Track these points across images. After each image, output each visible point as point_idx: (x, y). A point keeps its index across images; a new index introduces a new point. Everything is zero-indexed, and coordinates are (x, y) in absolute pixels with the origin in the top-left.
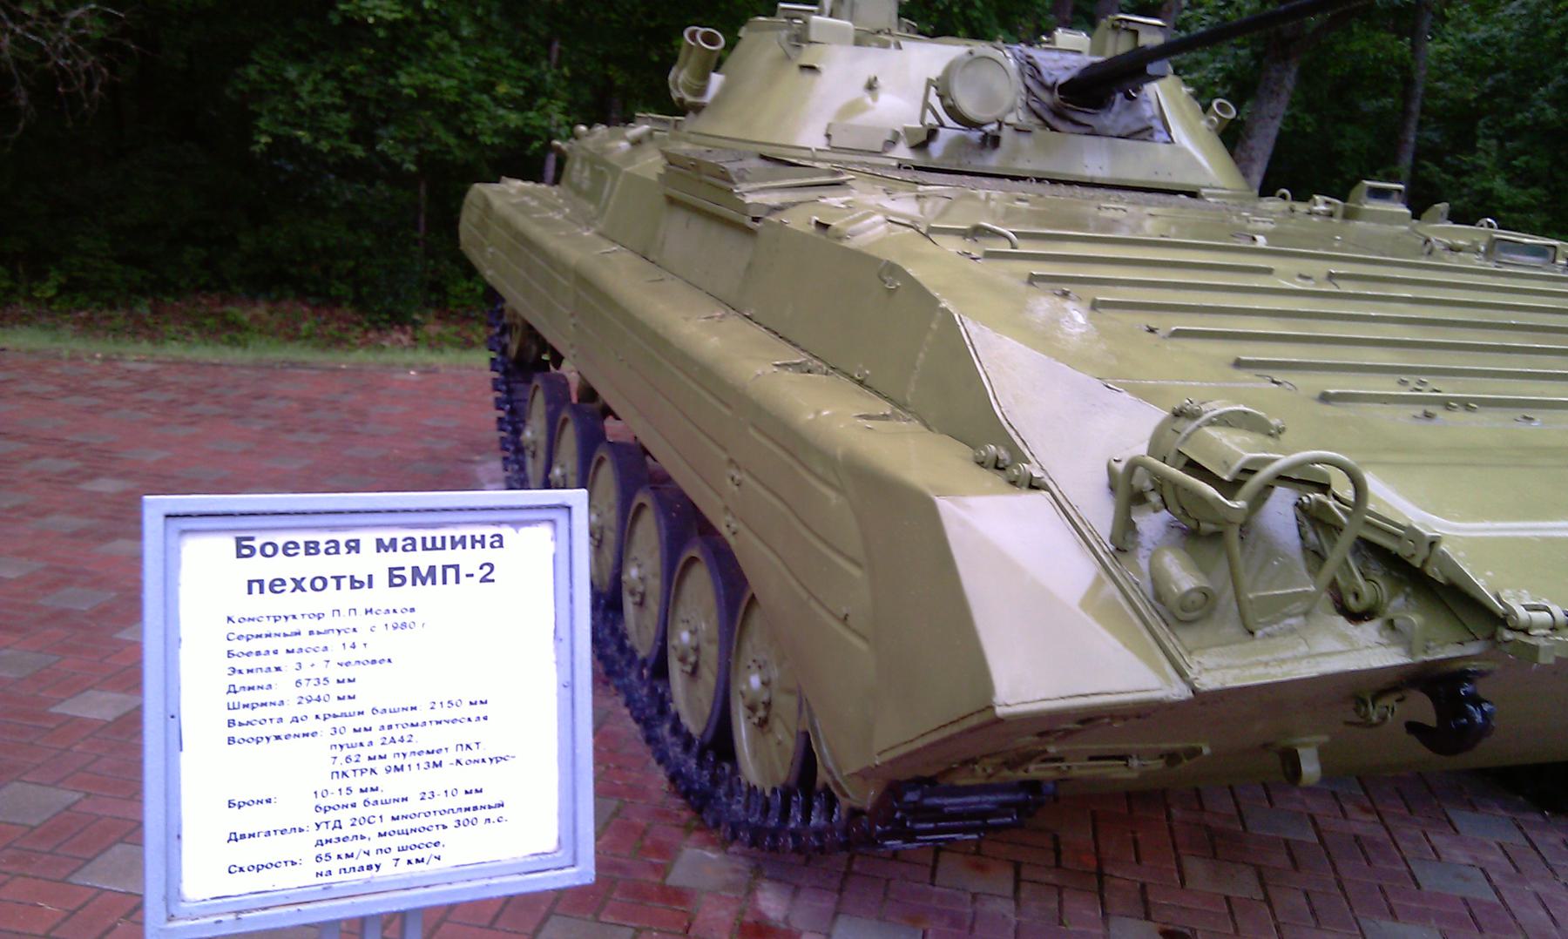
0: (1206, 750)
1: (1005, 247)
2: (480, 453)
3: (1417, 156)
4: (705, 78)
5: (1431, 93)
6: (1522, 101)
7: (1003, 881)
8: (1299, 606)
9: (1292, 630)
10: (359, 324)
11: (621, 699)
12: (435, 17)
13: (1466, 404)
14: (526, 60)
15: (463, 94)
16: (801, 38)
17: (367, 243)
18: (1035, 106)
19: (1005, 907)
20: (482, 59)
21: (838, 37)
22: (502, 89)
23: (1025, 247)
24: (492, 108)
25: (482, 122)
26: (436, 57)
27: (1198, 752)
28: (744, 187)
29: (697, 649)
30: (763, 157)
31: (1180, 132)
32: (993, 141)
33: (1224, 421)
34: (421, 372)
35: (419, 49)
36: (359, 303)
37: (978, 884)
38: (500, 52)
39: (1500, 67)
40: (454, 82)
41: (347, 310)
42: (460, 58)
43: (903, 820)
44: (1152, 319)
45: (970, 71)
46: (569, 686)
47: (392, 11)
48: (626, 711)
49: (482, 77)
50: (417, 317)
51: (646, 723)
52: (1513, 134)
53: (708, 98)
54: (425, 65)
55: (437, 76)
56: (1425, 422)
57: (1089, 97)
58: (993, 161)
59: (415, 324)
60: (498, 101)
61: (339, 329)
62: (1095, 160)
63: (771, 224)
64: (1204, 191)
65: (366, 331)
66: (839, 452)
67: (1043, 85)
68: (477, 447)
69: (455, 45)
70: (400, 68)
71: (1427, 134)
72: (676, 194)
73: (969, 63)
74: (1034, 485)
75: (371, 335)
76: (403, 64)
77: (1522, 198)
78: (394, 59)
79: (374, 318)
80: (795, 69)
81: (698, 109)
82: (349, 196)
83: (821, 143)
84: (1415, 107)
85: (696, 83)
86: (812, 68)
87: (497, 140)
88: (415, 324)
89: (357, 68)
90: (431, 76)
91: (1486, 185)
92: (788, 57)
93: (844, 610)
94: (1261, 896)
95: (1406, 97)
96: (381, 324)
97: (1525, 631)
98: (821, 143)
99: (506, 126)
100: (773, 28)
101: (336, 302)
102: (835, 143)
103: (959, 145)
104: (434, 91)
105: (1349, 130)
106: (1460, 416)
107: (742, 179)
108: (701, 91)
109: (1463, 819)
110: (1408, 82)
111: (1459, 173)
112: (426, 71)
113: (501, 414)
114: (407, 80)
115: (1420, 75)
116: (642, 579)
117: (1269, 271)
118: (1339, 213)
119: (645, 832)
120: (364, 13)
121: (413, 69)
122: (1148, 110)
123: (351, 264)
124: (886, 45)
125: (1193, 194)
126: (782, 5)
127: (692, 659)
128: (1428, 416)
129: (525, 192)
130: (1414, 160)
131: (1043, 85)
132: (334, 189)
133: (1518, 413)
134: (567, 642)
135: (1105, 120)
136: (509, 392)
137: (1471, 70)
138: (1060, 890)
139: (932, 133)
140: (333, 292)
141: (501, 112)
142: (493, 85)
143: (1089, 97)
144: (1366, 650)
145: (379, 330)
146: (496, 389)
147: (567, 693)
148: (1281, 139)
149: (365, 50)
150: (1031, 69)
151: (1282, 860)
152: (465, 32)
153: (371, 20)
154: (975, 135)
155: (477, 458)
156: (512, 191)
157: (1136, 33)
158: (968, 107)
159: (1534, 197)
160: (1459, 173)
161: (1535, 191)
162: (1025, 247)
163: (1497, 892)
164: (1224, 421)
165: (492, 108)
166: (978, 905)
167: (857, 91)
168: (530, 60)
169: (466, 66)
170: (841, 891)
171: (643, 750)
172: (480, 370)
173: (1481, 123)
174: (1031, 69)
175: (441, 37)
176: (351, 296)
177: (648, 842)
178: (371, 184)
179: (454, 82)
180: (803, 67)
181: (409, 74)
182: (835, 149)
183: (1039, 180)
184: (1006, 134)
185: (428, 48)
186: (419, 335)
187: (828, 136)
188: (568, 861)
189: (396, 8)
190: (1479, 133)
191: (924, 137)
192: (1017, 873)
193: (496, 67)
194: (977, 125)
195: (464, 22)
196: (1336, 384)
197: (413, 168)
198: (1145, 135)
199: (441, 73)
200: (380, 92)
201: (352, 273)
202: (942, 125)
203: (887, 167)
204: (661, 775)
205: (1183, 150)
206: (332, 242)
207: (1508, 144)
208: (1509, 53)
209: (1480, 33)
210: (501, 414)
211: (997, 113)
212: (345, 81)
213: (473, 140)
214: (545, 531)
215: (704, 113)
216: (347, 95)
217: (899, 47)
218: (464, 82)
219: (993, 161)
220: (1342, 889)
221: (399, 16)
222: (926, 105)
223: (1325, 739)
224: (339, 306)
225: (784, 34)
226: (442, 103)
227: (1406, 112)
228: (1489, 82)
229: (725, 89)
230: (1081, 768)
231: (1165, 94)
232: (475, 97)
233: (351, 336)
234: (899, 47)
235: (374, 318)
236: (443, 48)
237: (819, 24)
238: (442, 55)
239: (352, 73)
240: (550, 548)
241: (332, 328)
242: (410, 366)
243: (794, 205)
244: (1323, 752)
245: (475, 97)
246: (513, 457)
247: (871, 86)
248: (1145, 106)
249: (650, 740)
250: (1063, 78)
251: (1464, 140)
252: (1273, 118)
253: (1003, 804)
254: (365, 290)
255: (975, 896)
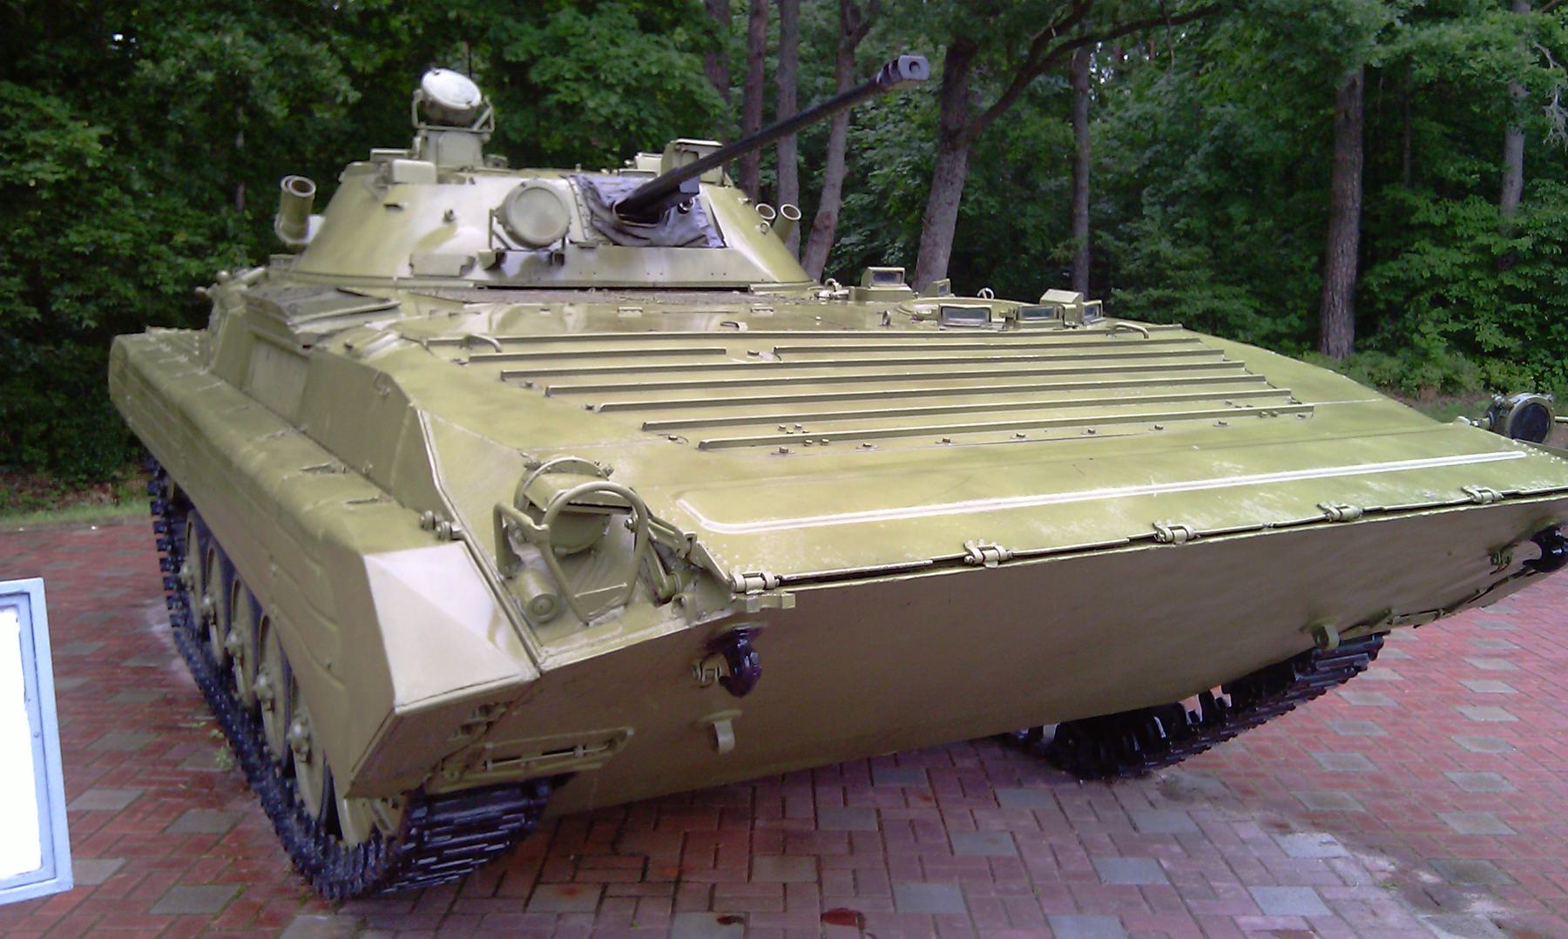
0: (630, 732)
1: (492, 352)
2: (152, 597)
3: (1093, 226)
4: (303, 221)
5: (1101, 168)
6: (1178, 168)
7: (590, 897)
8: (617, 600)
9: (615, 617)
10: (55, 487)
11: (258, 801)
12: (104, 174)
13: (819, 440)
14: (204, 208)
15: (138, 246)
16: (387, 180)
17: (58, 403)
18: (599, 225)
19: (585, 921)
20: (156, 210)
21: (421, 176)
22: (180, 238)
23: (509, 350)
24: (172, 258)
25: (161, 270)
26: (107, 213)
27: (623, 735)
28: (297, 319)
29: (308, 739)
30: (339, 291)
31: (737, 232)
32: (559, 258)
33: (558, 469)
34: (102, 527)
35: (88, 207)
36: (54, 465)
37: (565, 905)
38: (178, 201)
39: (1155, 140)
40: (128, 236)
41: (42, 475)
42: (132, 211)
43: (419, 837)
44: (590, 399)
45: (524, 200)
46: (39, 735)
47: (54, 173)
48: (262, 811)
49: (158, 228)
50: (117, 474)
51: (276, 817)
52: (1173, 199)
53: (310, 239)
54: (97, 222)
55: (109, 232)
56: (780, 457)
57: (648, 212)
58: (562, 276)
59: (114, 480)
60: (179, 252)
61: (34, 494)
62: (655, 267)
63: (318, 349)
64: (752, 287)
65: (64, 493)
66: (320, 533)
67: (602, 206)
68: (148, 592)
69: (127, 199)
70: (71, 227)
71: (1099, 207)
72: (261, 331)
73: (523, 194)
74: (454, 537)
75: (69, 498)
76: (73, 222)
77: (1185, 257)
78: (64, 219)
79: (72, 479)
80: (383, 209)
81: (297, 250)
82: (36, 360)
83: (405, 272)
84: (1084, 182)
85: (296, 227)
86: (396, 206)
87: (178, 289)
88: (114, 480)
89: (27, 231)
90: (103, 233)
91: (1154, 248)
92: (375, 199)
93: (327, 661)
94: (815, 878)
95: (1075, 174)
96: (79, 485)
97: (744, 592)
98: (405, 272)
99: (187, 274)
100: (365, 171)
101: (30, 467)
102: (417, 270)
103: (530, 264)
104: (107, 246)
105: (1030, 209)
106: (815, 449)
107: (295, 313)
108: (303, 233)
109: (1007, 795)
110: (1075, 161)
111: (1132, 240)
112: (98, 228)
113: (164, 554)
114: (78, 237)
115: (1085, 153)
116: (270, 686)
117: (723, 352)
118: (853, 296)
119: (261, 907)
120: (25, 177)
121: (83, 227)
122: (701, 222)
123: (43, 427)
124: (462, 181)
125: (744, 290)
126: (374, 151)
127: (305, 748)
128: (783, 452)
129: (168, 340)
130: (1091, 232)
131: (602, 206)
132: (18, 353)
133: (860, 443)
134: (35, 699)
135: (662, 232)
136: (171, 532)
137: (1132, 145)
138: (639, 898)
139: (500, 257)
140: (25, 458)
141: (181, 260)
142: (170, 236)
143: (648, 212)
144: (666, 623)
145: (77, 491)
146: (157, 531)
147: (39, 740)
148: (961, 219)
149: (31, 213)
150: (591, 192)
151: (843, 848)
152: (137, 187)
153: (32, 183)
154: (544, 254)
155: (149, 601)
156: (152, 339)
157: (696, 154)
158: (527, 231)
159: (1197, 254)
160: (1132, 240)
161: (1198, 249)
162: (509, 350)
163: (1018, 848)
164: (558, 469)
165: (172, 258)
166: (561, 922)
167: (435, 223)
168: (209, 207)
169: (141, 219)
170: (437, 929)
171: (273, 840)
172: (143, 517)
173: (1145, 192)
174: (591, 192)
175: (112, 192)
176: (45, 461)
177: (263, 915)
178: (58, 345)
179: (128, 236)
180: (388, 206)
181: (80, 233)
182: (418, 277)
183: (599, 289)
184: (570, 251)
185: (99, 206)
186: (120, 492)
187: (411, 265)
188: (49, 874)
189: (57, 169)
190: (1144, 201)
191: (493, 260)
192: (603, 892)
193: (173, 218)
194: (545, 246)
195: (135, 176)
196: (709, 436)
197: (93, 324)
198: (700, 242)
199: (114, 229)
200: (50, 253)
201: (44, 436)
202: (509, 249)
203: (466, 289)
204: (286, 860)
205: (735, 253)
206: (19, 407)
207: (1170, 209)
208: (1162, 127)
209: (1135, 110)
210: (164, 554)
211: (558, 232)
212: (12, 244)
213: (155, 290)
214: (10, 615)
215: (306, 254)
216: (15, 259)
217: (472, 182)
218: (140, 235)
219: (562, 276)
220: (887, 864)
221: (61, 177)
222: (492, 232)
223: (737, 712)
224: (33, 471)
225: (372, 178)
226: (117, 257)
227: (1076, 188)
228: (1148, 153)
229: (326, 228)
230: (540, 762)
231: (717, 200)
232: (152, 248)
233: (48, 501)
234: (472, 182)
235: (72, 479)
236: (114, 203)
237: (402, 167)
238: (114, 211)
239: (19, 236)
240: (17, 628)
241: (27, 495)
242: (92, 521)
243: (342, 331)
244: (737, 726)
245: (152, 248)
246: (177, 596)
247: (449, 218)
248: (698, 217)
249: (280, 830)
250: (620, 199)
251: (1132, 209)
252: (951, 204)
253: (508, 812)
254: (61, 452)
255: (560, 916)
